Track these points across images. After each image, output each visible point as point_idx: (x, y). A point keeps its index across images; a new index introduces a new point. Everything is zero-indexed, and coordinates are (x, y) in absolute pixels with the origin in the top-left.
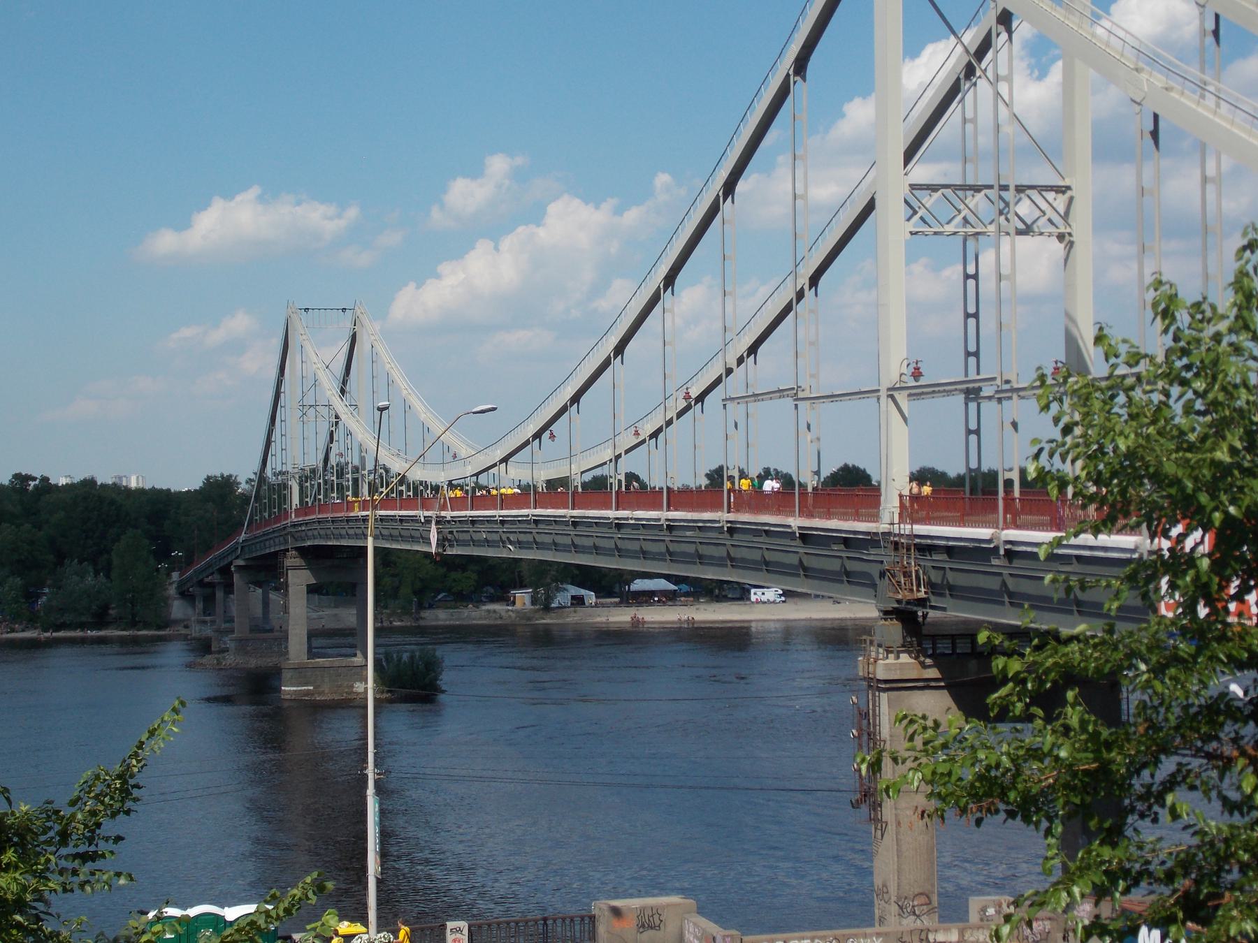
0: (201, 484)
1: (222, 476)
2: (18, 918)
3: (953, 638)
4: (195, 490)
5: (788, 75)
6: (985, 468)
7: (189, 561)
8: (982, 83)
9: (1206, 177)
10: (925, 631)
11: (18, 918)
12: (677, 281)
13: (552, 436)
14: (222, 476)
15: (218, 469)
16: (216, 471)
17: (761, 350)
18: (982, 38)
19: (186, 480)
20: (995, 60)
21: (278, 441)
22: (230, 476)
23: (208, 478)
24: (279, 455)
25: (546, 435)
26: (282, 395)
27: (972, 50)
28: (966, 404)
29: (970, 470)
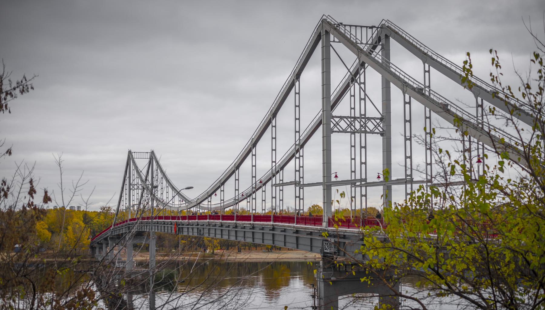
13: (216, 195)
20: (360, 77)
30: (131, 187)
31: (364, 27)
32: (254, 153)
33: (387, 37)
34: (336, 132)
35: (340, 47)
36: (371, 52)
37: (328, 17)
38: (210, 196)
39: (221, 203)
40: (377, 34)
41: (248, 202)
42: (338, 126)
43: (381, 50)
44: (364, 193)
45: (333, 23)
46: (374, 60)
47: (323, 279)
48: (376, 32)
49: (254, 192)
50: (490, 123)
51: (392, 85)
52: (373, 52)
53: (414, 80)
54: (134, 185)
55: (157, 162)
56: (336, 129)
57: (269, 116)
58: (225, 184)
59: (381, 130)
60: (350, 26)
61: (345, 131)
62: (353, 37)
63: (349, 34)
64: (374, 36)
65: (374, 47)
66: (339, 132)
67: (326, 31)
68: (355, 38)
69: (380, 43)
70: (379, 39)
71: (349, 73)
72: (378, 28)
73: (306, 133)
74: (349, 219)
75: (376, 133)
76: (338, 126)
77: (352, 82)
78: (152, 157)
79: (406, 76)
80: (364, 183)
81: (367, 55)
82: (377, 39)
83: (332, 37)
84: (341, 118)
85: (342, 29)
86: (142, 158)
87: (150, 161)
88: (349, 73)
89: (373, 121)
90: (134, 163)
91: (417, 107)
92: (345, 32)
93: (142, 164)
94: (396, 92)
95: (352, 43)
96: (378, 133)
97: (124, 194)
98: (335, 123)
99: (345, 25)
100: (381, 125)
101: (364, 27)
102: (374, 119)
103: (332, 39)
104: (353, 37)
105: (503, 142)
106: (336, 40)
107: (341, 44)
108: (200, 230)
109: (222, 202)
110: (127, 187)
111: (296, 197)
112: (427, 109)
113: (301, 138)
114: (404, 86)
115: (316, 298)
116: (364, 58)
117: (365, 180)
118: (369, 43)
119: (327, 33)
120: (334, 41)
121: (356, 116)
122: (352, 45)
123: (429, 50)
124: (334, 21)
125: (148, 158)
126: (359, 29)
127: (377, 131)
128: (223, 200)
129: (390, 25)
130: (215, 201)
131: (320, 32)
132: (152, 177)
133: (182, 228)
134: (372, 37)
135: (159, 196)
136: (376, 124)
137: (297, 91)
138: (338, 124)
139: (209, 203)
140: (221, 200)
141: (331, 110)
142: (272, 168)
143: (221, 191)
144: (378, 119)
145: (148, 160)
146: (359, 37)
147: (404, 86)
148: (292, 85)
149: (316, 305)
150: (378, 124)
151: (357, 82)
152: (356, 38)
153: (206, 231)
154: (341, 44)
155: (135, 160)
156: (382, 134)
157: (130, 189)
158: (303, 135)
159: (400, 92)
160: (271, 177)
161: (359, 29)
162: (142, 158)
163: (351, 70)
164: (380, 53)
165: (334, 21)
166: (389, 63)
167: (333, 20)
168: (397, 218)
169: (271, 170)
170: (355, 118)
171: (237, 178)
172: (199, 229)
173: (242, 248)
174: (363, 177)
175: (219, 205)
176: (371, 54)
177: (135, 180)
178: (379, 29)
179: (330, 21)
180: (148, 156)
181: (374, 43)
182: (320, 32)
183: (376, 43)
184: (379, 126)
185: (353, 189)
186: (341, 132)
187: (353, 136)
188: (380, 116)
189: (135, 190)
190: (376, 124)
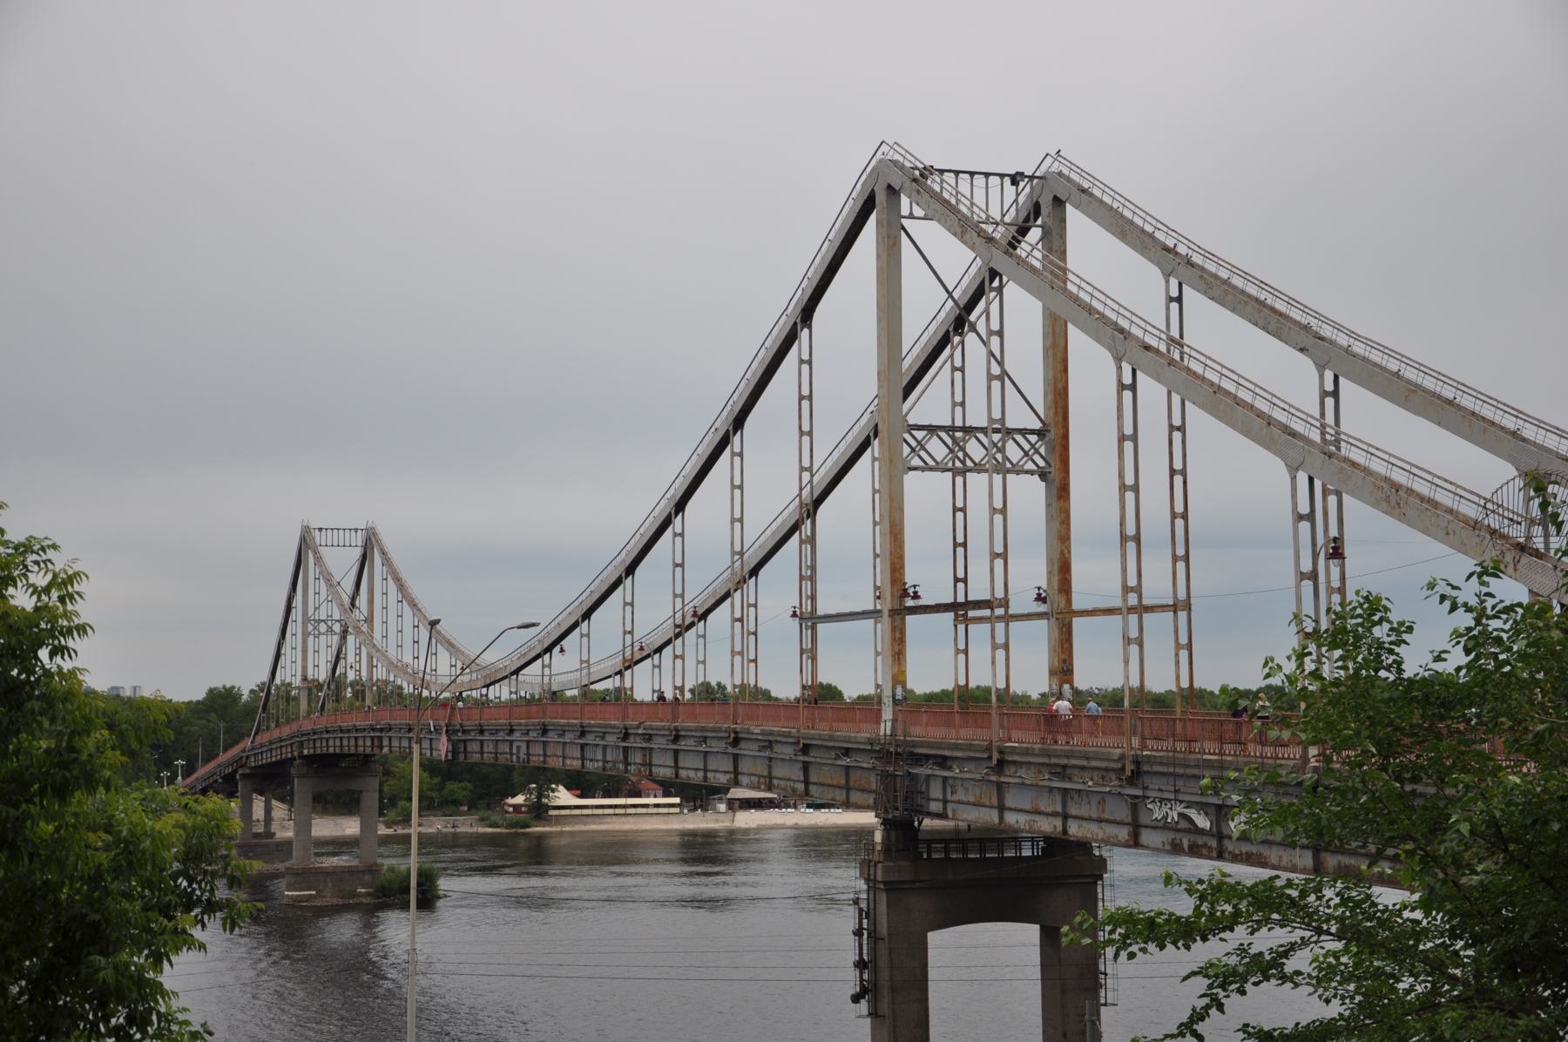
0: (205, 695)
1: (224, 687)
2: (91, 1017)
3: (946, 841)
4: (198, 702)
5: (795, 324)
6: (972, 685)
7: (189, 770)
8: (971, 338)
9: (1124, 485)
10: (921, 836)
11: (91, 1017)
12: (687, 508)
13: (562, 650)
14: (224, 687)
15: (220, 682)
16: (218, 683)
17: (762, 573)
18: (862, 440)
19: (187, 689)
20: (987, 311)
21: (288, 653)
22: (233, 687)
23: (211, 691)
24: (288, 668)
25: (557, 649)
26: (294, 610)
27: (962, 303)
28: (956, 626)
29: (959, 687)
30: (310, 628)
32: (679, 530)
33: (1058, 203)
34: (915, 469)
35: (930, 234)
36: (1013, 244)
37: (895, 147)
38: (549, 649)
39: (581, 669)
40: (1030, 195)
41: (654, 666)
42: (923, 453)
43: (1041, 239)
44: (1000, 639)
45: (908, 164)
46: (1022, 262)
47: (885, 883)
48: (1028, 189)
49: (677, 636)
51: (1072, 330)
52: (1019, 242)
53: (1158, 221)
54: (320, 621)
55: (387, 561)
56: (916, 462)
57: (723, 424)
59: (1042, 463)
60: (957, 173)
61: (939, 467)
62: (949, 189)
63: (968, 203)
64: (1022, 199)
65: (1023, 231)
66: (926, 468)
67: (889, 187)
68: (954, 192)
69: (1039, 222)
70: (1036, 210)
72: (1032, 178)
73: (829, 463)
75: (1027, 472)
76: (923, 453)
77: (956, 330)
78: (370, 547)
79: (1122, 311)
80: (996, 608)
81: (1006, 252)
82: (1030, 206)
83: (905, 201)
84: (932, 429)
85: (934, 183)
86: (335, 544)
87: (364, 557)
88: (950, 303)
89: (1019, 438)
90: (318, 559)
91: (1151, 391)
92: (973, 212)
93: (342, 562)
94: (1085, 351)
95: (946, 203)
96: (1031, 473)
97: (286, 649)
98: (914, 443)
99: (942, 171)
100: (1042, 451)
102: (1024, 432)
103: (905, 211)
104: (949, 189)
105: (1288, 430)
106: (918, 212)
107: (934, 225)
108: (518, 747)
110: (295, 627)
112: (1176, 399)
114: (1116, 336)
115: (865, 936)
116: (1000, 262)
117: (1005, 603)
118: (1007, 219)
119: (893, 192)
120: (911, 216)
121: (956, 425)
122: (965, 227)
123: (1181, 239)
124: (913, 160)
125: (360, 544)
126: (979, 181)
127: (1030, 466)
128: (588, 661)
129: (1066, 171)
130: (564, 669)
131: (873, 190)
132: (371, 601)
133: (465, 741)
134: (1016, 201)
135: (392, 652)
136: (1027, 447)
137: (805, 357)
138: (923, 448)
140: (582, 662)
142: (800, 495)
143: (582, 636)
144: (1032, 432)
145: (358, 552)
146: (979, 199)
147: (1116, 336)
148: (790, 339)
149: (866, 958)
150: (1033, 446)
151: (973, 328)
152: (957, 193)
154: (934, 224)
155: (323, 551)
156: (1043, 475)
157: (305, 635)
158: (823, 471)
159: (448, 654)
161: (979, 181)
162: (335, 544)
163: (956, 295)
164: (1040, 246)
165: (913, 160)
166: (1065, 270)
167: (908, 156)
170: (969, 430)
171: (629, 600)
172: (515, 745)
174: (1000, 594)
176: (1015, 248)
177: (323, 608)
178: (1036, 181)
179: (901, 159)
180: (359, 539)
181: (1021, 219)
182: (873, 190)
183: (1027, 220)
184: (1037, 451)
185: (961, 627)
186: (931, 469)
187: (959, 480)
188: (1037, 425)
189: (323, 638)
190: (1027, 447)
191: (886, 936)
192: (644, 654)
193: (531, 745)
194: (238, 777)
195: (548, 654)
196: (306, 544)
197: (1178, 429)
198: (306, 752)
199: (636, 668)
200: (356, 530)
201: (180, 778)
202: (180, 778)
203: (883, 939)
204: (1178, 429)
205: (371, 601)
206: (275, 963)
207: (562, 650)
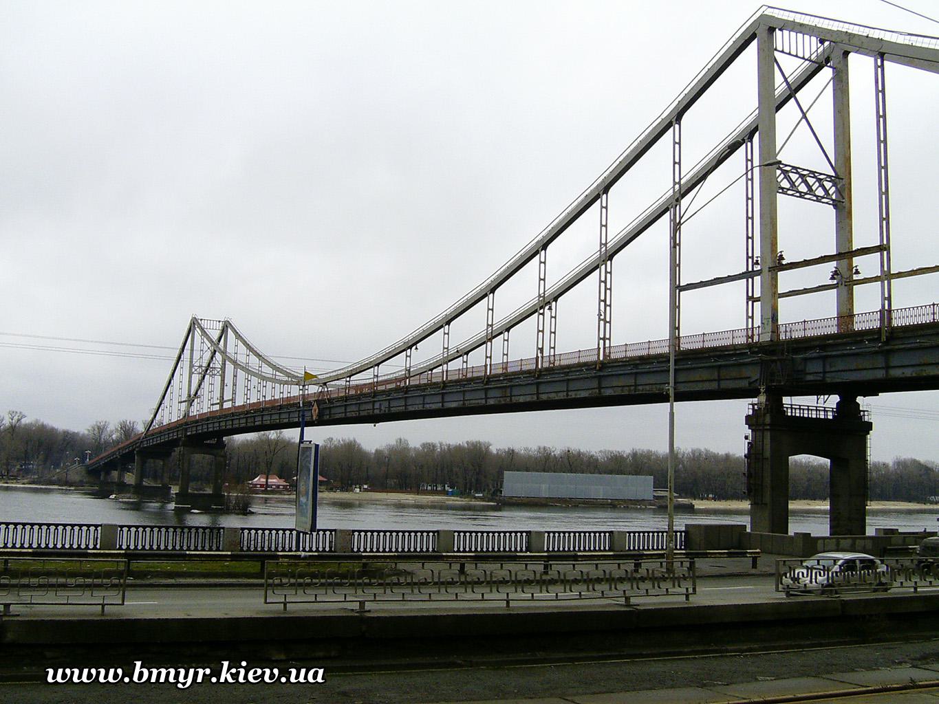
13: (416, 348)
25: (414, 347)
31: (799, 57)
38: (410, 347)
50: (745, 172)
58: (615, 258)
71: (785, 84)
74: (209, 483)
101: (799, 57)
109: (446, 350)
111: (610, 322)
113: (682, 182)
132: (190, 382)
134: (817, 51)
139: (348, 383)
141: (776, 112)
142: (600, 250)
153: (789, 410)
160: (598, 265)
168: (253, 513)
169: (599, 253)
173: (102, 478)
175: (371, 381)
185: (750, 303)
191: (769, 457)
192: (459, 354)
193: (391, 402)
194: (135, 452)
195: (409, 350)
196: (194, 324)
197: (540, 331)
198: (188, 434)
199: (449, 363)
200: (219, 321)
201: (88, 460)
202: (88, 460)
203: (767, 459)
204: (540, 331)
205: (190, 382)
206: (437, 466)
207: (416, 348)
